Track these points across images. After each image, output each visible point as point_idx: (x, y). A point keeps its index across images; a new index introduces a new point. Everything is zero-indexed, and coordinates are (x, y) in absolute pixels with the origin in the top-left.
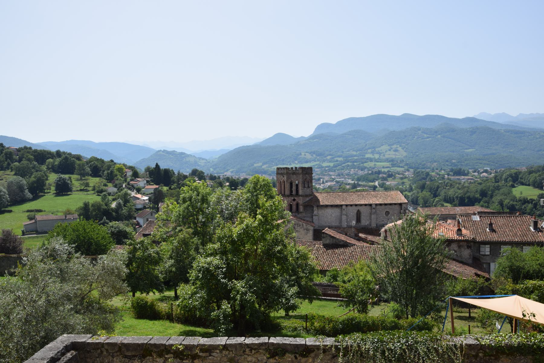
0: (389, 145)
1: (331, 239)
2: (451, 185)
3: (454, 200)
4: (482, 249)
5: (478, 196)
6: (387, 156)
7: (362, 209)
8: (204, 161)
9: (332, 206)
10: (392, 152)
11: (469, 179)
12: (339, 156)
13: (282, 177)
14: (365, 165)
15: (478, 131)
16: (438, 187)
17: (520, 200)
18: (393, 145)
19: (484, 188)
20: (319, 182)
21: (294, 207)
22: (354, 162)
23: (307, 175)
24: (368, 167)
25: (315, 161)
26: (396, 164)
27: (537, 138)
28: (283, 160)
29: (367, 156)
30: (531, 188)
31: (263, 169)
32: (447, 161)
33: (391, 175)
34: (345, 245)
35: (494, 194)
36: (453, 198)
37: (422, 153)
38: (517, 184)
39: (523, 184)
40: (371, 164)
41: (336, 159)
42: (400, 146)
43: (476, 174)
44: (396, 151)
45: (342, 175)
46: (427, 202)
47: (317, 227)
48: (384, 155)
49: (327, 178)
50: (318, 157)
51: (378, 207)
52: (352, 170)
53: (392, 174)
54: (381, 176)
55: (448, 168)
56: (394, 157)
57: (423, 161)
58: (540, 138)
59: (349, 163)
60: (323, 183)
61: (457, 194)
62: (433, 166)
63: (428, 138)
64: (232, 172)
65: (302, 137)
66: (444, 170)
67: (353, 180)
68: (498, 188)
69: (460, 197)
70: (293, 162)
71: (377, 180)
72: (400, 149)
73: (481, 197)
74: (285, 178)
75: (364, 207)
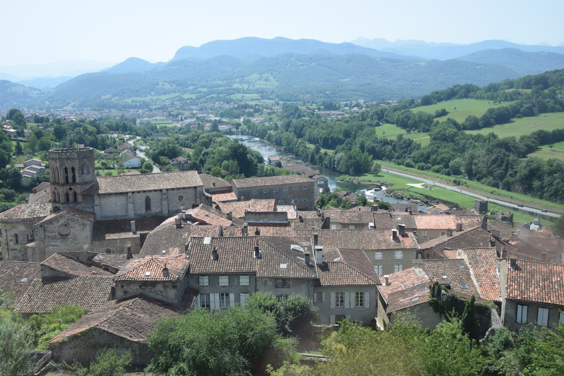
0: (259, 74)
1: (51, 271)
2: (317, 123)
3: (318, 140)
4: (201, 280)
5: (341, 136)
6: (257, 87)
7: (151, 195)
8: (37, 92)
9: (116, 194)
10: (263, 82)
11: (339, 115)
13: (54, 162)
14: (232, 97)
15: (355, 59)
16: (303, 126)
17: (381, 142)
18: (263, 73)
20: (177, 119)
21: (71, 198)
23: (85, 160)
24: (235, 99)
25: (175, 92)
26: (265, 96)
27: (412, 68)
28: (137, 91)
29: (235, 86)
30: (394, 126)
32: (321, 92)
34: (66, 277)
35: (358, 134)
36: (317, 138)
38: (382, 122)
39: (388, 122)
40: (238, 96)
41: (199, 89)
42: (271, 75)
43: (347, 108)
44: (267, 80)
45: (205, 109)
46: (290, 143)
47: (99, 218)
48: (254, 86)
49: (187, 113)
50: (179, 88)
51: (169, 192)
52: (217, 103)
54: (247, 110)
56: (264, 87)
57: (296, 92)
59: (214, 95)
60: (182, 120)
61: (321, 135)
62: (305, 98)
63: (302, 65)
64: (74, 106)
65: (160, 63)
66: (316, 103)
67: (216, 116)
68: (361, 128)
69: (324, 138)
70: (149, 93)
71: (242, 115)
72: (271, 78)
73: (344, 138)
74: (58, 163)
75: (154, 193)
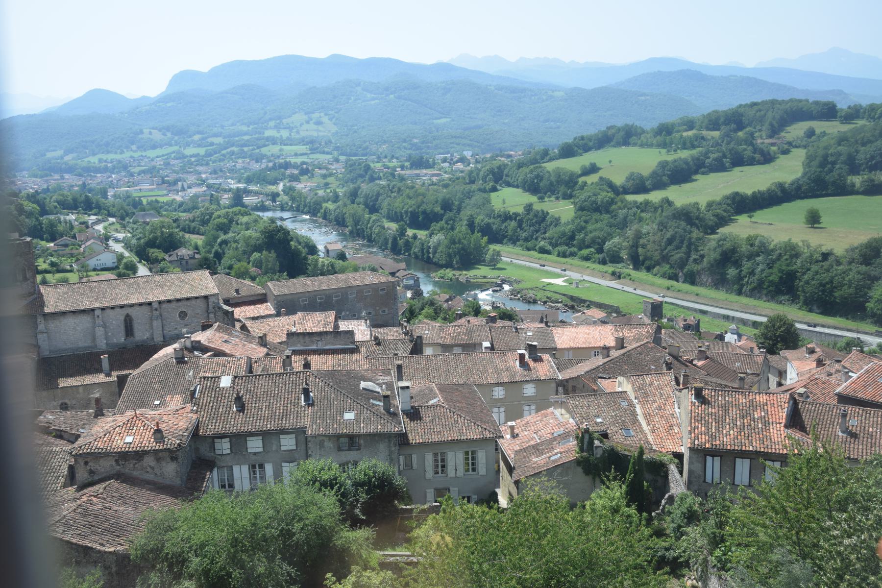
0: (306, 114)
2: (399, 189)
4: (217, 446)
5: (438, 209)
7: (133, 312)
10: (312, 126)
11: (434, 175)
12: (215, 135)
16: (378, 195)
17: (499, 216)
19: (448, 196)
20: (175, 188)
22: (243, 146)
24: (269, 154)
25: (171, 145)
26: (317, 148)
27: (543, 101)
28: (107, 144)
29: (268, 133)
31: (65, 163)
32: (405, 141)
33: (305, 171)
35: (463, 205)
36: (401, 213)
37: (363, 127)
39: (509, 185)
40: (275, 149)
41: (210, 140)
42: (326, 115)
43: (446, 165)
44: (319, 123)
45: (221, 171)
47: (46, 353)
48: (298, 132)
49: (191, 179)
50: (176, 138)
52: (240, 161)
53: (307, 169)
54: (288, 172)
55: (404, 154)
56: (315, 134)
57: (365, 142)
58: (547, 100)
59: (235, 149)
60: (183, 189)
61: (406, 207)
62: (380, 150)
63: (373, 99)
66: (397, 158)
67: (239, 182)
68: (469, 195)
69: (411, 212)
71: (281, 180)
72: (325, 119)
73: (442, 212)
75: (138, 308)
